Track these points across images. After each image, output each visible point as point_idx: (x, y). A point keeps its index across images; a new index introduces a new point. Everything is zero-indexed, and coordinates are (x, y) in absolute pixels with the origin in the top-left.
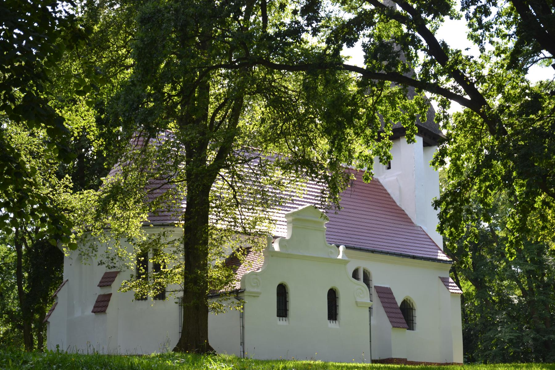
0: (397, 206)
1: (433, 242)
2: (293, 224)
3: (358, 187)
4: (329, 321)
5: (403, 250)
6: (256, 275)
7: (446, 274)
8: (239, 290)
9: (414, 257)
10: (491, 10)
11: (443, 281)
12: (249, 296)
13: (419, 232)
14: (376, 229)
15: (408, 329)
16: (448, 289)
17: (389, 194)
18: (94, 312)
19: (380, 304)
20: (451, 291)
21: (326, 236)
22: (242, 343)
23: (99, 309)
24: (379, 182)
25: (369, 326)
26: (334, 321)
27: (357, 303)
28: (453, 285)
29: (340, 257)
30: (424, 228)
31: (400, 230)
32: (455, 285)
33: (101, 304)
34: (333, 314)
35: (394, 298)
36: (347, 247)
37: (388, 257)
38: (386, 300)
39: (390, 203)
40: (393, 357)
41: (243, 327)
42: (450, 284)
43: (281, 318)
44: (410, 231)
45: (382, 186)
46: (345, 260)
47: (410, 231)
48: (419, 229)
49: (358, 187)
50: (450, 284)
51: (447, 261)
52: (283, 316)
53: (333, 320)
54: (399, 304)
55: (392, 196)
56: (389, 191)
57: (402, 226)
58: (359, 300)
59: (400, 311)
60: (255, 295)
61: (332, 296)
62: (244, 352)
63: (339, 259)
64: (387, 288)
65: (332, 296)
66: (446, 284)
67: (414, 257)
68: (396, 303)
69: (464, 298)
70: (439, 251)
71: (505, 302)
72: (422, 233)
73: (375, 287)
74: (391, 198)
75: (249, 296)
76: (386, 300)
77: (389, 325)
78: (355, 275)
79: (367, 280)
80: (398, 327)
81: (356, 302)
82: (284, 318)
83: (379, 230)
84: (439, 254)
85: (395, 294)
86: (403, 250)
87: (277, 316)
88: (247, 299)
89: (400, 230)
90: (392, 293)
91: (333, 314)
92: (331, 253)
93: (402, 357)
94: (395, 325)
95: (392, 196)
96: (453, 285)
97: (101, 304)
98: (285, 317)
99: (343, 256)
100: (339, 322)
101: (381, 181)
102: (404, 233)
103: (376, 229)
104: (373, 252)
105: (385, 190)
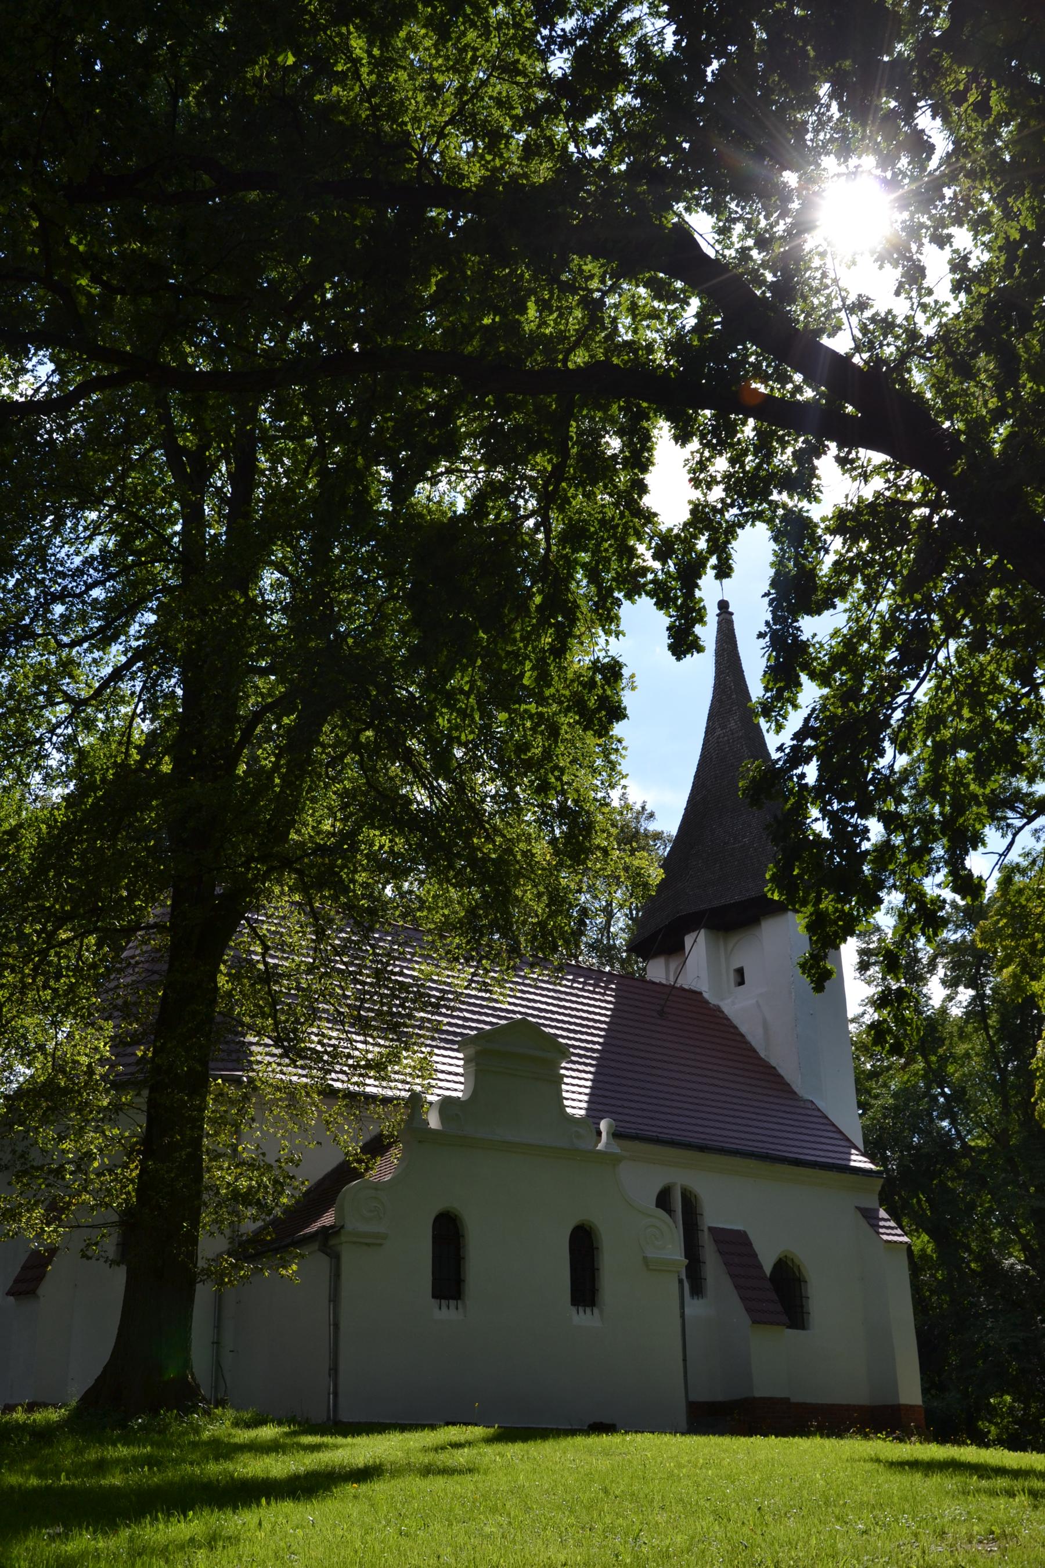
0: (761, 1059)
1: (841, 1132)
2: (477, 1064)
4: (574, 1309)
6: (376, 1189)
7: (871, 1201)
8: (332, 1227)
11: (864, 1217)
12: (355, 1243)
13: (809, 1112)
14: (714, 1104)
15: (789, 1327)
16: (879, 1233)
17: (742, 1036)
20: (885, 1237)
22: (334, 1370)
25: (678, 1321)
26: (588, 1310)
27: (646, 1261)
28: (887, 1224)
30: (820, 1104)
31: (767, 1106)
32: (892, 1224)
35: (755, 1255)
37: (737, 1161)
41: (336, 1326)
42: (882, 1223)
44: (788, 1109)
45: (728, 1019)
46: (612, 1154)
47: (788, 1109)
48: (809, 1105)
50: (882, 1223)
51: (870, 1171)
53: (585, 1306)
54: (768, 1269)
55: (749, 1038)
56: (743, 1029)
57: (771, 1099)
62: (336, 1395)
66: (873, 1222)
67: (797, 1163)
68: (760, 1267)
69: (916, 1263)
70: (853, 1151)
71: (992, 1272)
72: (816, 1113)
73: (710, 1229)
74: (747, 1043)
75: (355, 1243)
78: (663, 1200)
80: (772, 1323)
81: (645, 1258)
82: (452, 1303)
83: (720, 1104)
84: (853, 1157)
85: (758, 1247)
87: (434, 1296)
88: (349, 1257)
89: (767, 1106)
90: (750, 1244)
94: (759, 1317)
95: (749, 1038)
96: (887, 1224)
99: (607, 1143)
101: (726, 1009)
102: (774, 1113)
103: (714, 1104)
104: (702, 1148)
105: (736, 1028)
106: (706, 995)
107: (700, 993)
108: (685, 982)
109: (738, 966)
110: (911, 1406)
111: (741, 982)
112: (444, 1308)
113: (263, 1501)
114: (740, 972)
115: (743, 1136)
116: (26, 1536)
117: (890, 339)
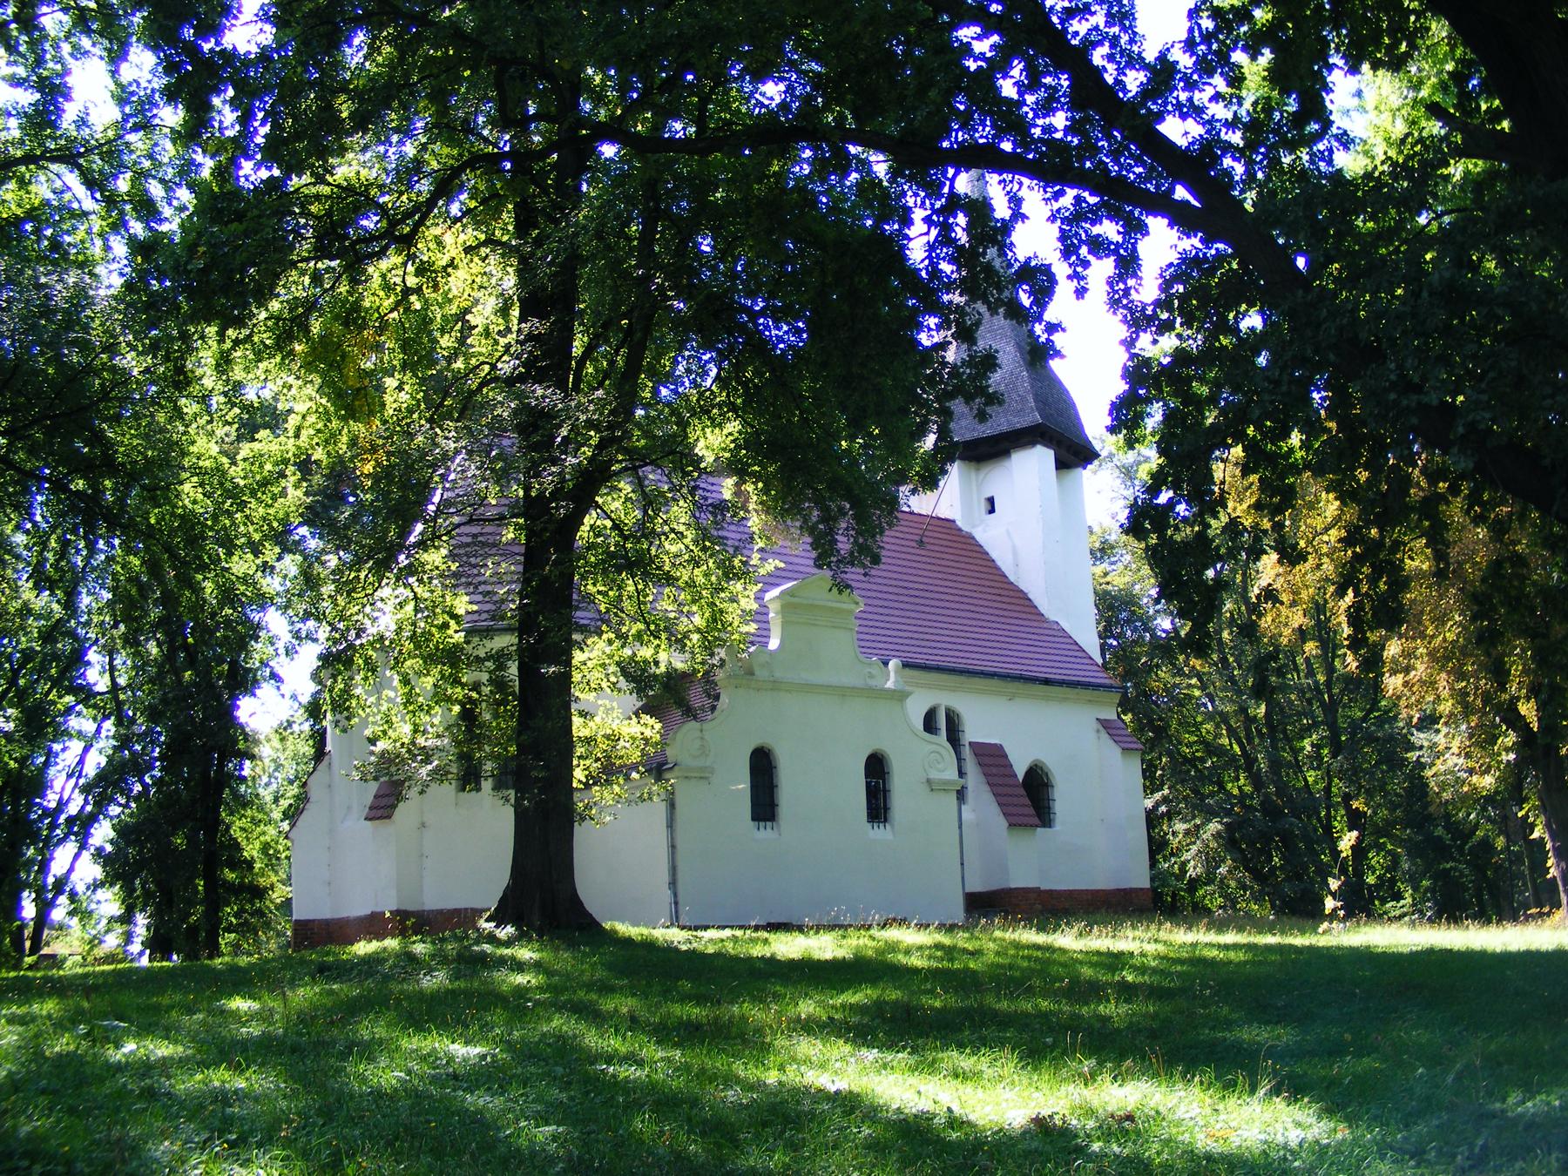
3: (929, 547)
4: (870, 825)
5: (1025, 668)
9: (1047, 682)
10: (1125, 328)
18: (370, 819)
19: (982, 779)
21: (856, 636)
23: (380, 813)
24: (973, 538)
29: (890, 685)
33: (384, 802)
34: (878, 808)
36: (906, 665)
37: (995, 682)
38: (994, 771)
39: (997, 578)
40: (1013, 885)
41: (673, 846)
43: (762, 824)
49: (929, 547)
52: (765, 820)
54: (1021, 777)
58: (934, 775)
59: (1022, 791)
60: (703, 776)
61: (876, 767)
63: (889, 690)
64: (995, 745)
65: (876, 767)
67: (1047, 682)
74: (998, 568)
76: (994, 771)
77: (1002, 822)
78: (930, 724)
79: (954, 736)
81: (928, 781)
82: (769, 824)
85: (1012, 757)
86: (1025, 668)
89: (1002, 639)
90: (1006, 756)
91: (878, 808)
92: (871, 676)
93: (1031, 886)
95: (999, 563)
97: (384, 802)
98: (769, 820)
99: (896, 682)
100: (893, 827)
101: (978, 538)
106: (959, 523)
107: (954, 521)
108: (943, 512)
109: (989, 495)
110: (1142, 889)
111: (992, 511)
112: (769, 829)
113: (803, 1016)
114: (991, 501)
115: (927, 609)
116: (376, 1020)
117: (1335, 273)
